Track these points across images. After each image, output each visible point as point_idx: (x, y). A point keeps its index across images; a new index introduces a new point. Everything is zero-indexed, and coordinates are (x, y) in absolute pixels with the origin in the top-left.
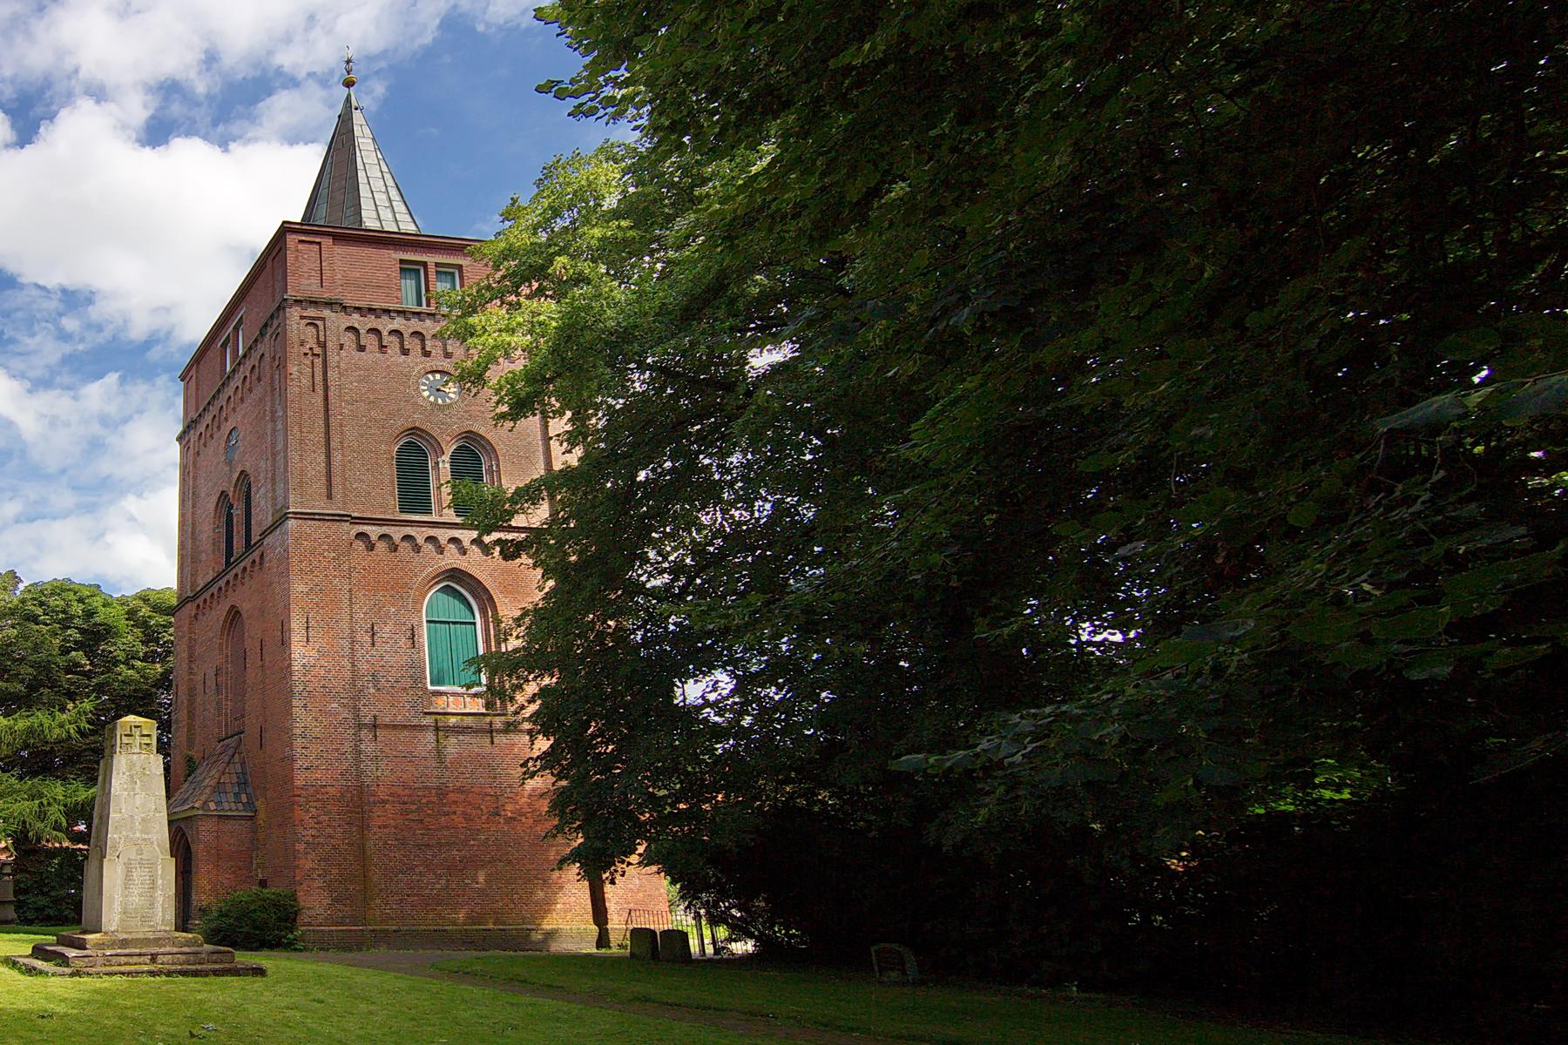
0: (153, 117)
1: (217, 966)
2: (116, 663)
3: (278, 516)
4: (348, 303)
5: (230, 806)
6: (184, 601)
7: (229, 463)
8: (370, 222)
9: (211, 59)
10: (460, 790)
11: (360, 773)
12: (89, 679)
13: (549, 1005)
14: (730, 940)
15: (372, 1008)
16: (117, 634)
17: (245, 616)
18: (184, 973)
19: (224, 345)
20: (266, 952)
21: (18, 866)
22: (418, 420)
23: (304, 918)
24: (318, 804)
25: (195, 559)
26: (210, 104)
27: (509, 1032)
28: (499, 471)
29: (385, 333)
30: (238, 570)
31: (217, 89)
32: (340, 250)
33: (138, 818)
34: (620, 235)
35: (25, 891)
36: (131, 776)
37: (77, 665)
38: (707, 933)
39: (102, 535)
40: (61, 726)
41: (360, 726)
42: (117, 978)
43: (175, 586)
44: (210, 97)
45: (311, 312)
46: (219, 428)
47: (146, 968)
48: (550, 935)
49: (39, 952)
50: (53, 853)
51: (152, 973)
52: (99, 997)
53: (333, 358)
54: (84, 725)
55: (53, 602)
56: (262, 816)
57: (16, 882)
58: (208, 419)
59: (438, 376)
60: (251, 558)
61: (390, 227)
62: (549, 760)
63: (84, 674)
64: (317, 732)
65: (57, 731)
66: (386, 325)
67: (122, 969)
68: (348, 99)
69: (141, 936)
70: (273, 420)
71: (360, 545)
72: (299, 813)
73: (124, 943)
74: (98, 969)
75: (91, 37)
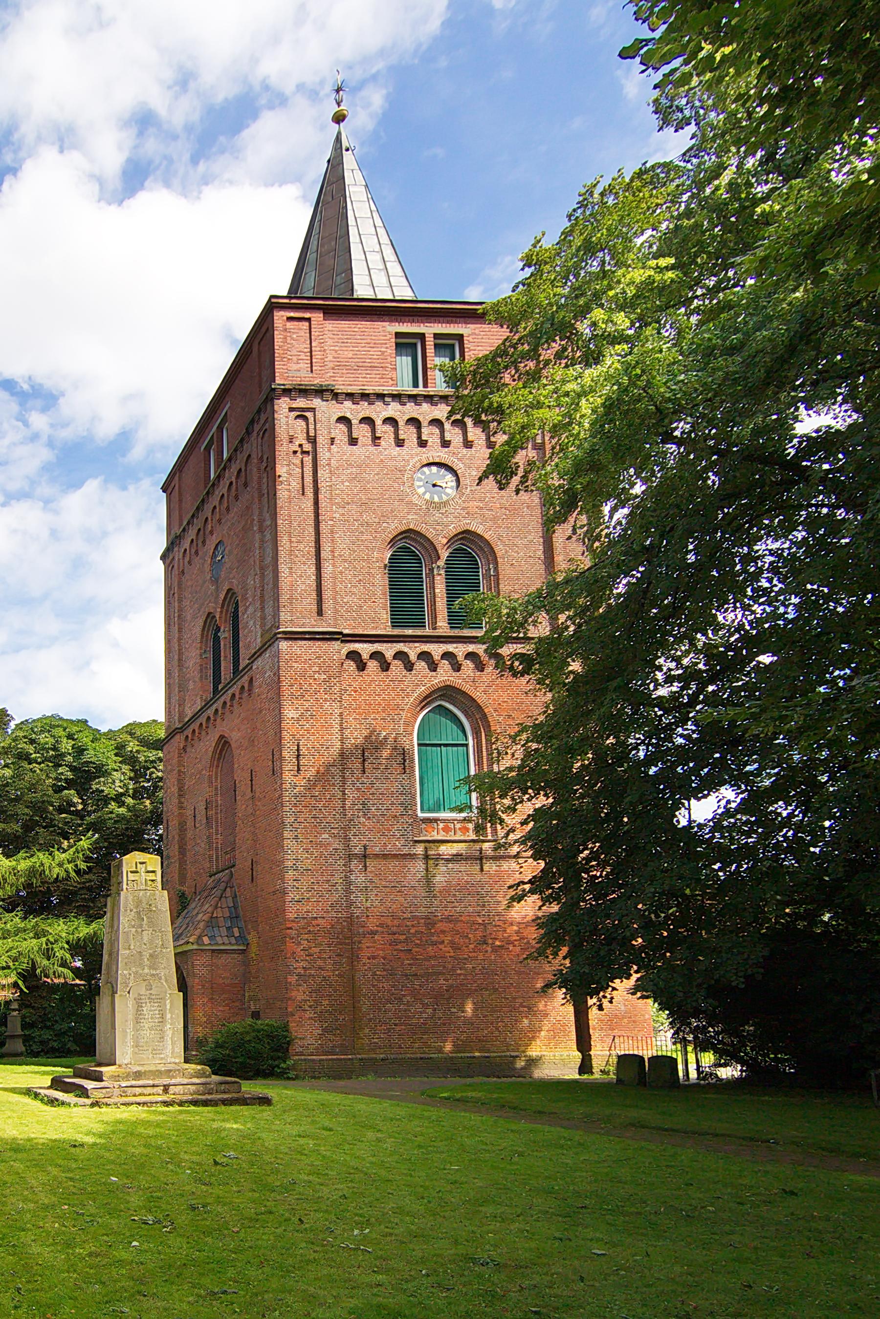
0: (129, 161)
1: (226, 1096)
2: (106, 800)
3: (268, 636)
4: (340, 388)
5: (223, 942)
6: (172, 734)
7: (215, 581)
8: (362, 290)
9: (184, 81)
10: (449, 919)
11: (350, 904)
12: (82, 818)
13: (550, 1132)
14: (718, 1065)
15: (379, 1135)
16: (107, 774)
17: (233, 745)
18: (195, 1103)
19: (208, 449)
20: (260, 1081)
21: (24, 1001)
22: (412, 521)
23: (296, 1047)
24: (310, 937)
25: (182, 688)
26: (187, 138)
27: (516, 1159)
28: (497, 575)
29: (378, 422)
30: (227, 697)
31: (196, 117)
32: (331, 325)
33: (146, 955)
34: (658, 278)
35: (32, 1025)
36: (138, 913)
37: (71, 804)
38: (691, 1057)
39: (88, 663)
40: (60, 865)
41: (350, 857)
42: (133, 1108)
43: (161, 717)
44: (189, 128)
45: (301, 403)
46: (204, 542)
47: (160, 1098)
48: (533, 1062)
49: (57, 1083)
50: (54, 988)
51: (166, 1104)
52: (121, 1127)
53: (323, 455)
54: (83, 866)
55: (44, 738)
56: (254, 949)
57: (23, 1017)
58: (192, 534)
59: (434, 469)
60: (239, 684)
61: (384, 294)
62: (539, 884)
63: (77, 813)
64: (308, 864)
65: (56, 870)
66: (380, 412)
67: (138, 1099)
68: (338, 139)
69: (153, 1068)
70: (261, 530)
71: (351, 665)
72: (290, 945)
73: (138, 1075)
74: (116, 1100)
75: (51, 67)
